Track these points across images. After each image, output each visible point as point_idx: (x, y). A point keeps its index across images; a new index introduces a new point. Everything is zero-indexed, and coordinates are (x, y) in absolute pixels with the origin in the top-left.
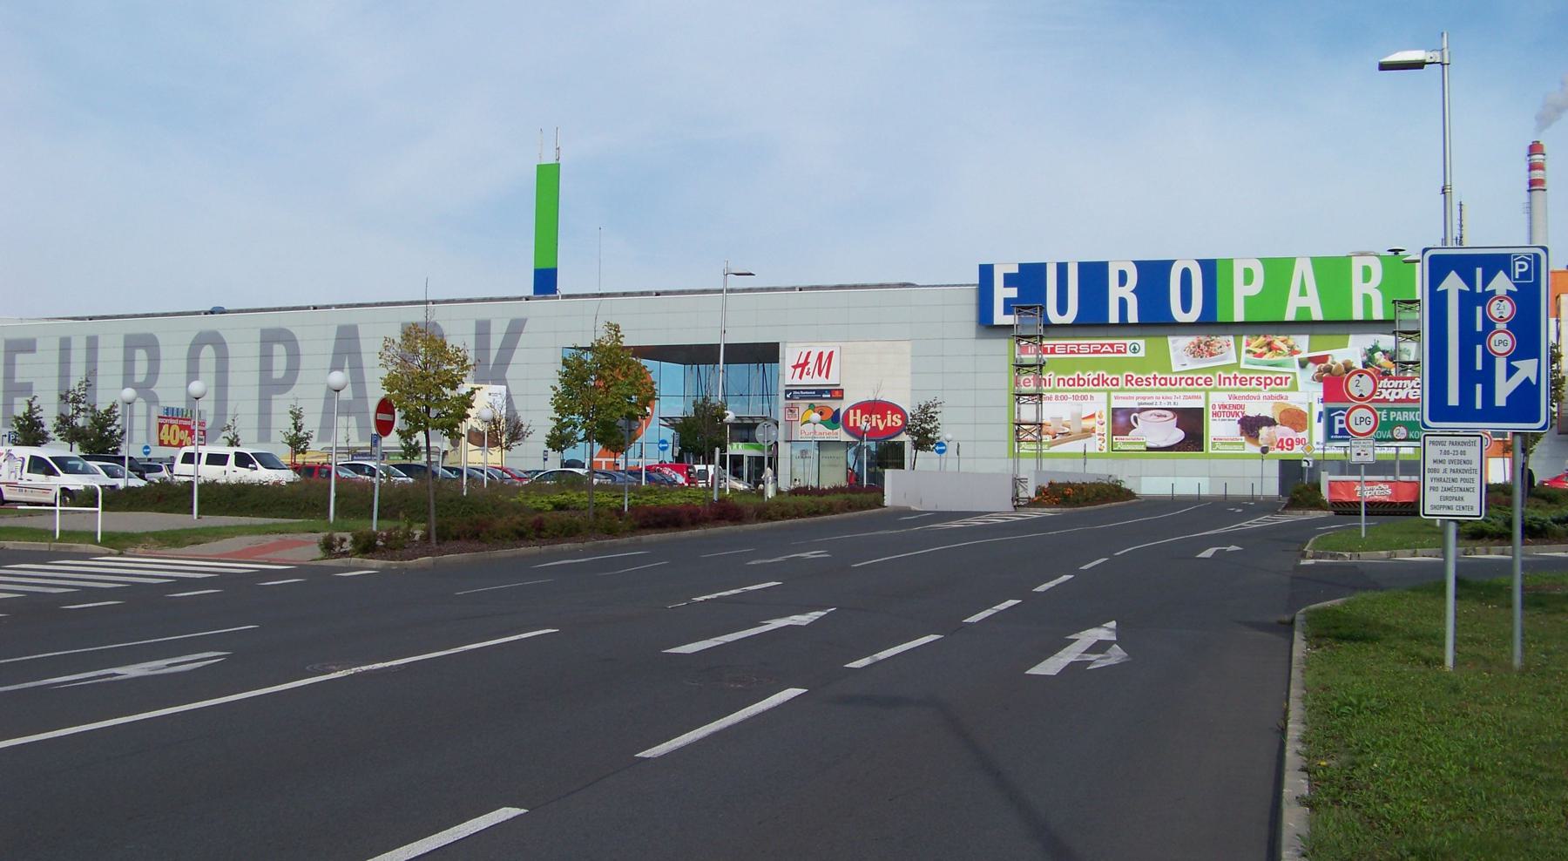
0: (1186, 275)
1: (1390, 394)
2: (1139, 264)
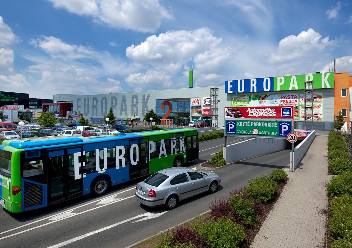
0: (267, 81)
1: (256, 114)
2: (257, 79)
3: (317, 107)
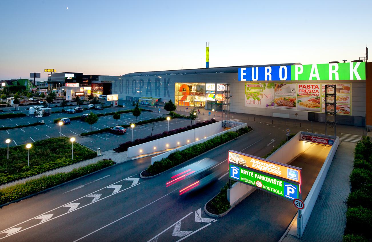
1: (260, 167)
3: (343, 99)
